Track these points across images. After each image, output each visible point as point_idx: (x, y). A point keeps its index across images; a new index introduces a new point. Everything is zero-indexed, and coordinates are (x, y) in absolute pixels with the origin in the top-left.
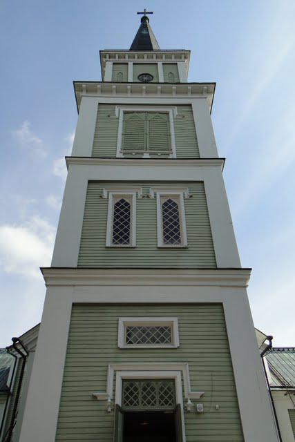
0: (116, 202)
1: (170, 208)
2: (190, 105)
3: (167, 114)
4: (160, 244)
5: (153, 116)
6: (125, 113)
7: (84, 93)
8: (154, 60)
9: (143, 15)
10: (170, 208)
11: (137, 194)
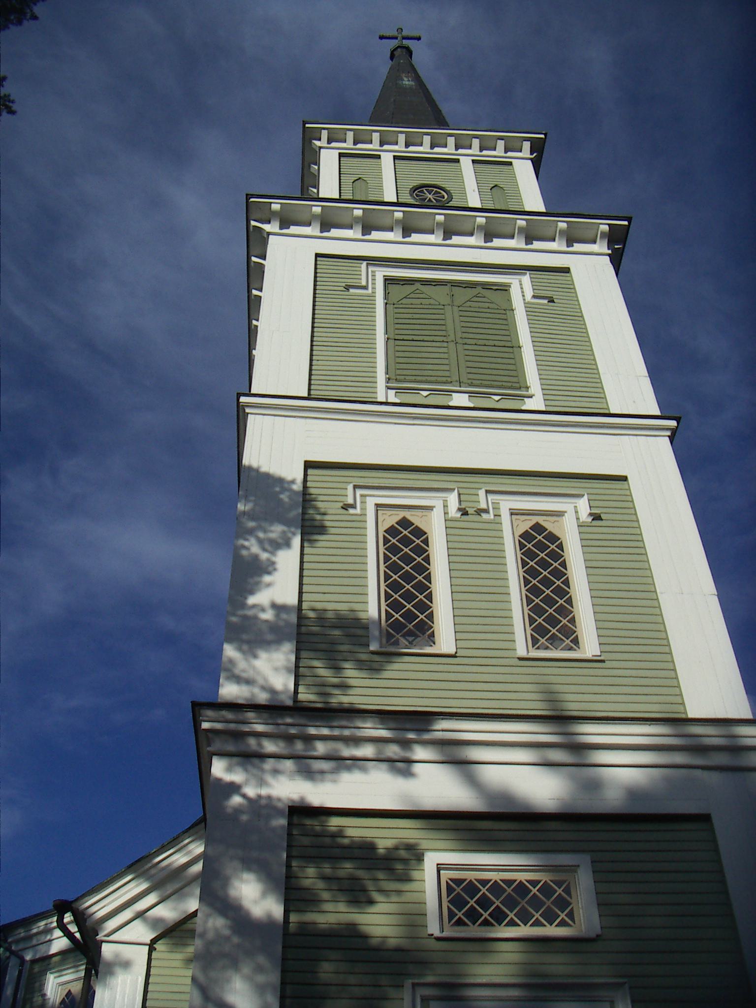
0: (521, 530)
1: (541, 553)
2: (567, 270)
3: (504, 289)
4: (521, 651)
5: (471, 292)
6: (388, 281)
7: (271, 227)
8: (449, 150)
9: (394, 43)
10: (541, 553)
11: (445, 506)
